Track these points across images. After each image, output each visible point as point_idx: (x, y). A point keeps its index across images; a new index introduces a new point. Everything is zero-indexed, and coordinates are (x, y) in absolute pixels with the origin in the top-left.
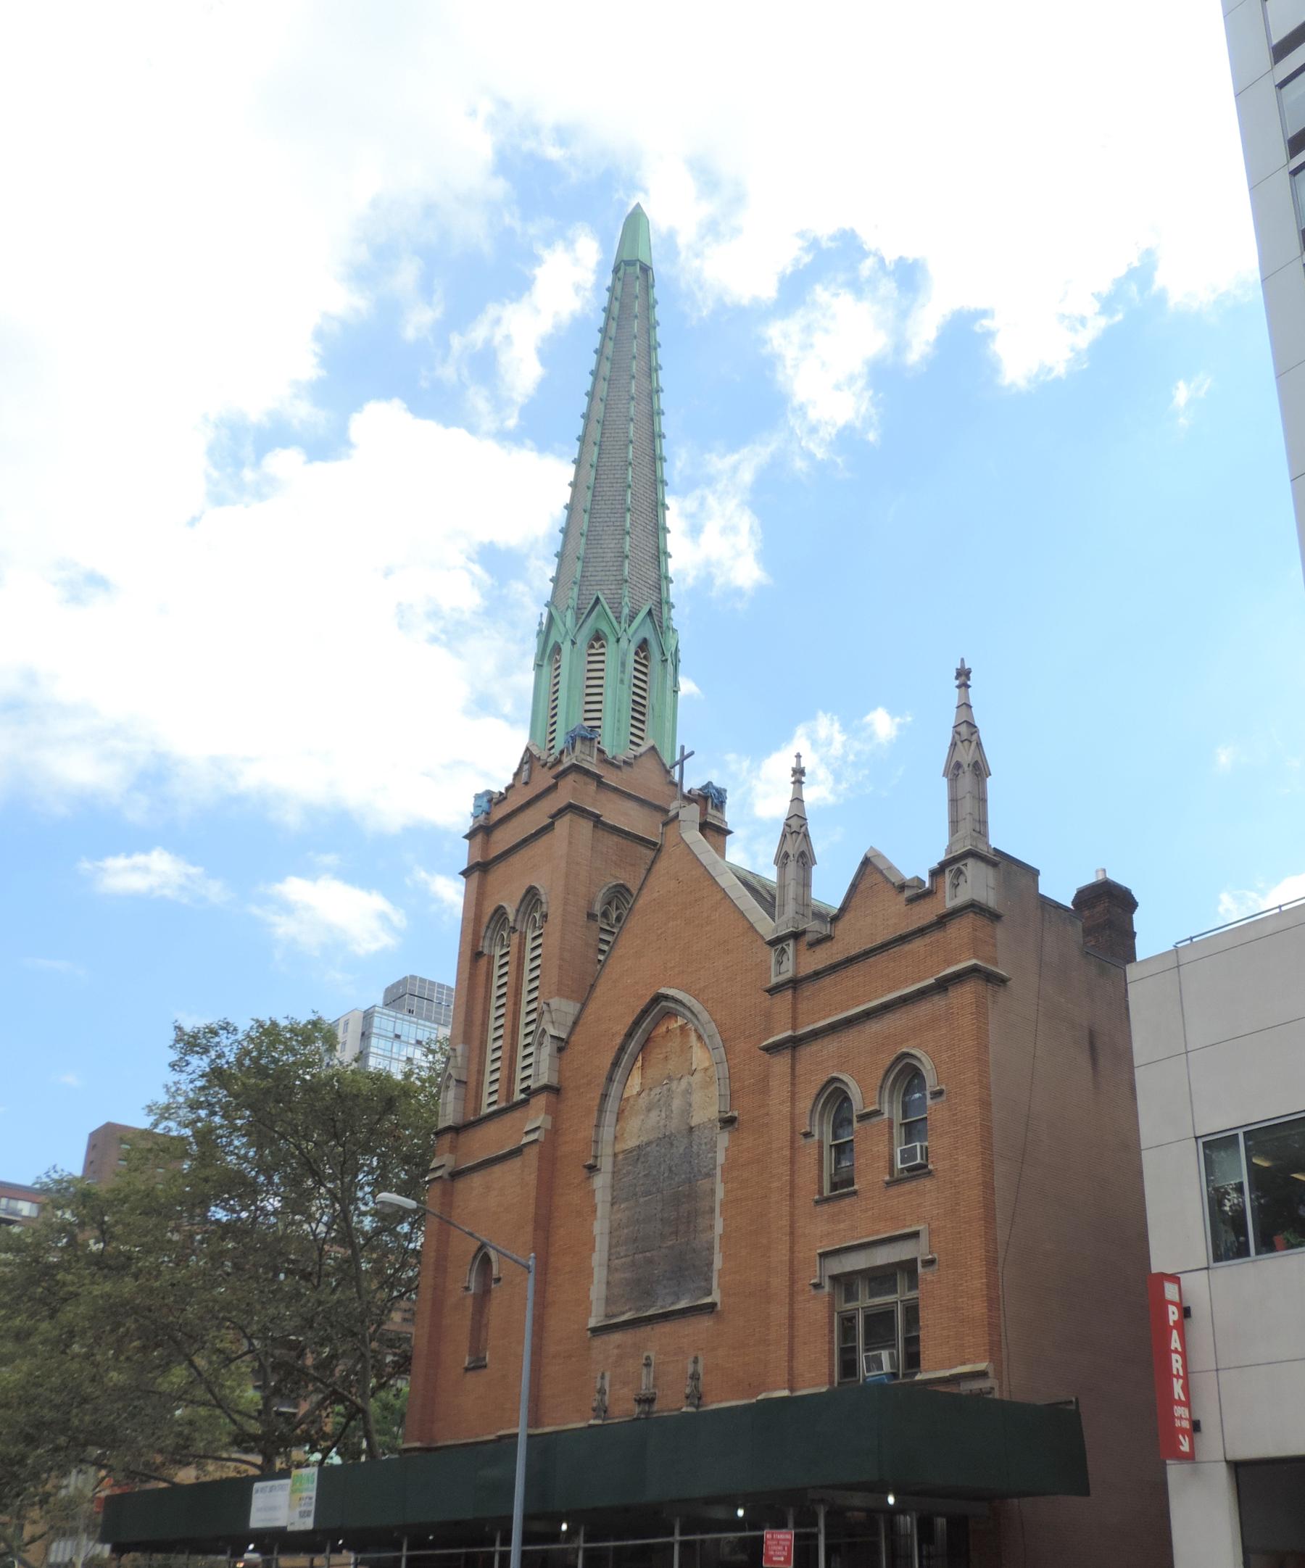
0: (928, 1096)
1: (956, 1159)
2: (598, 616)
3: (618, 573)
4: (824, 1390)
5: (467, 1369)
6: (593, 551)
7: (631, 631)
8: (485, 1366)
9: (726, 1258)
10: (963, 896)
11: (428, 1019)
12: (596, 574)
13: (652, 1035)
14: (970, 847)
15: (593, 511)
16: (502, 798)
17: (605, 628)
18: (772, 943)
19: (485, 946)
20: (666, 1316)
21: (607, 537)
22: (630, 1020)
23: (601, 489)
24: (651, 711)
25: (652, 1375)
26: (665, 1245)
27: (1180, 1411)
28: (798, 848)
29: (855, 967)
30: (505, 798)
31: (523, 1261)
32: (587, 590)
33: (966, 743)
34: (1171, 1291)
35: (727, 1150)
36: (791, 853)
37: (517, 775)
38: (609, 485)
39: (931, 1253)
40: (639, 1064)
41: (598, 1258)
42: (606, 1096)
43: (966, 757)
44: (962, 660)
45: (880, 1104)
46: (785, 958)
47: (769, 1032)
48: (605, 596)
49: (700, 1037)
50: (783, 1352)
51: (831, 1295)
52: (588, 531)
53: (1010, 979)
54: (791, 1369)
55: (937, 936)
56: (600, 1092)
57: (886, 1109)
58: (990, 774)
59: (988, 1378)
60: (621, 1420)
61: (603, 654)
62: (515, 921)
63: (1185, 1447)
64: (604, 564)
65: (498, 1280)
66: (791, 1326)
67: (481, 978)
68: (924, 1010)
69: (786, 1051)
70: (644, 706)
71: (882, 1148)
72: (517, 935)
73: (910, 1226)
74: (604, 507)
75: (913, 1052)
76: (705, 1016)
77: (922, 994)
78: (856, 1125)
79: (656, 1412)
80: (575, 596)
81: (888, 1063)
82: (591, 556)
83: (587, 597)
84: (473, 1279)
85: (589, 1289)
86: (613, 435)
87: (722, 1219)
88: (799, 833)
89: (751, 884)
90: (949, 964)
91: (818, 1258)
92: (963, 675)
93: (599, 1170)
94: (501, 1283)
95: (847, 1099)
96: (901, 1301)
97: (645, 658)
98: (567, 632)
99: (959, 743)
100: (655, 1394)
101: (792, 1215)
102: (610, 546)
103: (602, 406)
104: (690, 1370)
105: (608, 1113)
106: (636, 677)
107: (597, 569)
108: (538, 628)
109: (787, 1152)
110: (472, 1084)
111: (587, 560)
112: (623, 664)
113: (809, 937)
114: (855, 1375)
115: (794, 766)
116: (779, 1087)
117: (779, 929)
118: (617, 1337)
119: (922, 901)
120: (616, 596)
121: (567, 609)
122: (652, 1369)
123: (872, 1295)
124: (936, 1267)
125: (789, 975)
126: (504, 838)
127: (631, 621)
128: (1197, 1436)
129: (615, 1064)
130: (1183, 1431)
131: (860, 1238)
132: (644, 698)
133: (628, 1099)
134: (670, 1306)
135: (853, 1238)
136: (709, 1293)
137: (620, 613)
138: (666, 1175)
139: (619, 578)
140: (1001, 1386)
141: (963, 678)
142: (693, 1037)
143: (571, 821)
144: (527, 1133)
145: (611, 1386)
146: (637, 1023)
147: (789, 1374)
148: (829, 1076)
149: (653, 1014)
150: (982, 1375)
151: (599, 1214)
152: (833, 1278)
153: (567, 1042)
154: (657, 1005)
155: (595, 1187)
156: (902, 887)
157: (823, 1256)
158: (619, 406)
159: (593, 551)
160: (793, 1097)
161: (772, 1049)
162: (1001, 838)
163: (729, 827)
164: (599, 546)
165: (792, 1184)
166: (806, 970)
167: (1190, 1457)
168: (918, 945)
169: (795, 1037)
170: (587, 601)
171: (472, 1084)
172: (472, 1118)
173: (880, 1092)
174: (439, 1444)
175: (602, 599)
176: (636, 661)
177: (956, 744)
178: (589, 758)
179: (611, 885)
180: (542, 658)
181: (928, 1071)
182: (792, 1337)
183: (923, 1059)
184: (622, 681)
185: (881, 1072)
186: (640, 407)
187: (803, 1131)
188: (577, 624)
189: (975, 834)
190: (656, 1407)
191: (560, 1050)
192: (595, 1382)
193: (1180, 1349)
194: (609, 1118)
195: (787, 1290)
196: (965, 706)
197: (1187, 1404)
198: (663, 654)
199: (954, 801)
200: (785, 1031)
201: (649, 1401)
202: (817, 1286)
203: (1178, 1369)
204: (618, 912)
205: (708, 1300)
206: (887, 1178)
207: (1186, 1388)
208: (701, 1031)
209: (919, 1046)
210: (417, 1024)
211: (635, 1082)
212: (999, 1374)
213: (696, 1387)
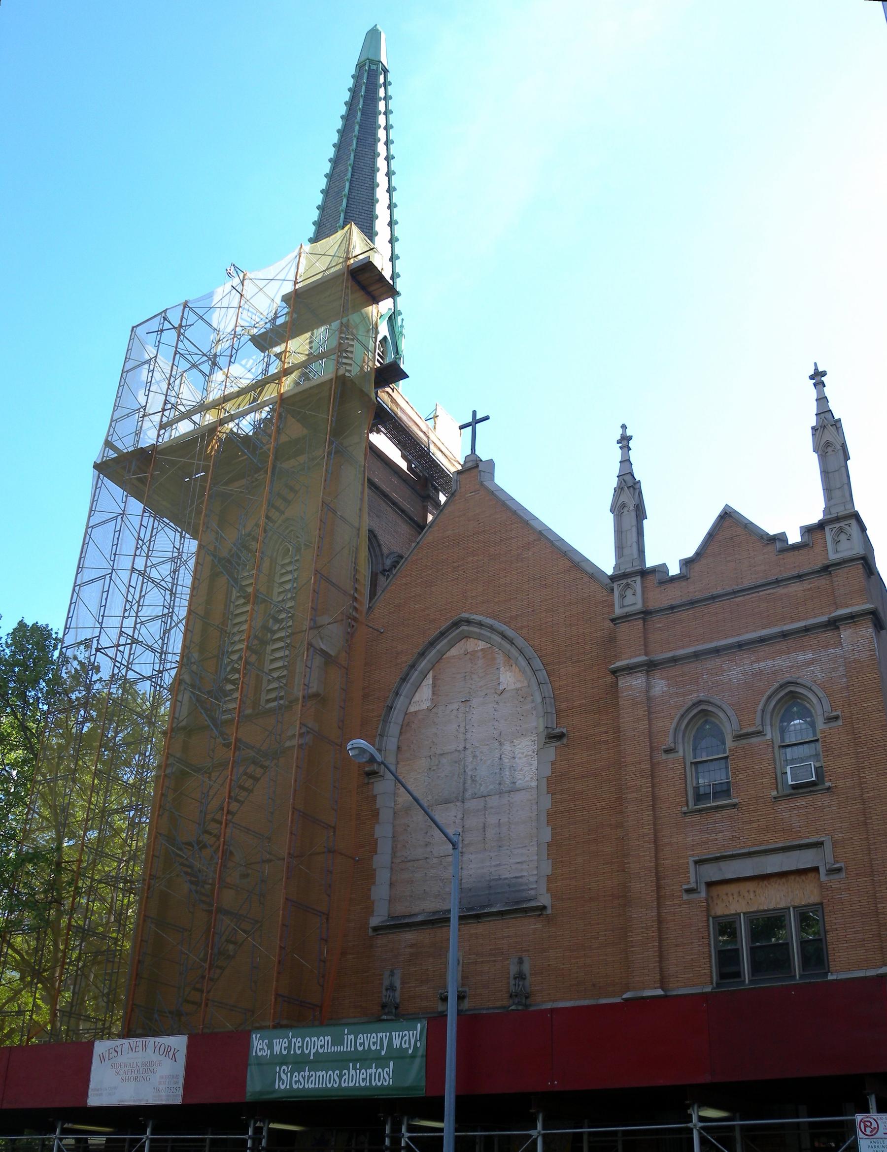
4: (708, 989)
40: (429, 680)
42: (391, 708)
44: (815, 364)
45: (763, 726)
57: (768, 730)
73: (807, 837)
86: (361, 178)
92: (625, 441)
96: (794, 908)
104: (513, 969)
125: (639, 606)
145: (403, 983)
149: (450, 637)
154: (457, 629)
158: (366, 159)
195: (654, 894)
206: (774, 793)
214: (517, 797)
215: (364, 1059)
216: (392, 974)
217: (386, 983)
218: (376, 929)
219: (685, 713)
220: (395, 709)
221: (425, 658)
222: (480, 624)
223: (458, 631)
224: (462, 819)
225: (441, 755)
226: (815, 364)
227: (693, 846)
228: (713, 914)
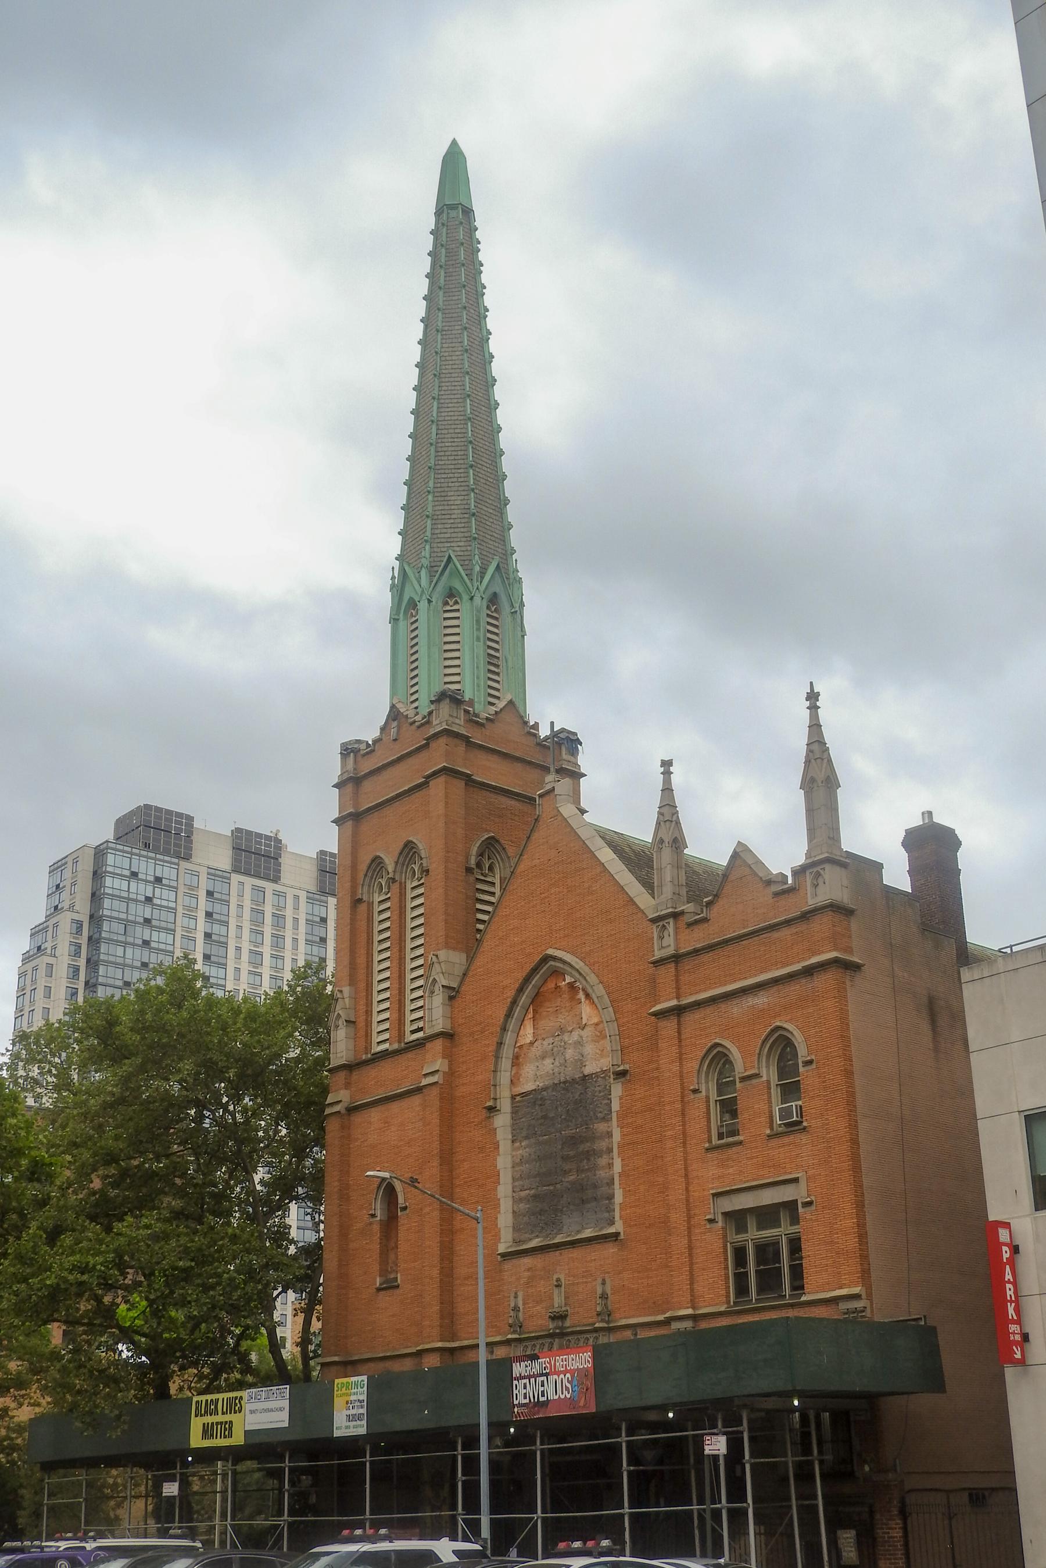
0: (801, 1064)
1: (827, 1119)
2: (451, 574)
3: (465, 530)
5: (379, 1290)
7: (482, 588)
8: (398, 1286)
9: (626, 1193)
11: (166, 852)
13: (541, 990)
16: (371, 749)
17: (458, 585)
18: (654, 921)
19: (362, 893)
20: (573, 1244)
21: (452, 493)
22: (521, 975)
24: (505, 664)
25: (563, 1295)
26: (567, 1180)
27: (1013, 1328)
29: (730, 948)
30: (373, 751)
31: (473, 1214)
34: (1003, 1235)
35: (621, 1098)
37: (383, 729)
38: (450, 440)
39: (809, 1196)
40: (530, 1015)
41: (504, 1190)
43: (820, 776)
44: (811, 683)
46: (666, 933)
48: (456, 554)
49: (588, 996)
51: (724, 1229)
53: (863, 965)
54: (692, 1290)
55: (802, 927)
56: (496, 1039)
57: (764, 1072)
60: (537, 1334)
61: (458, 610)
62: (394, 872)
63: (1018, 1356)
65: (405, 1208)
66: (690, 1255)
67: (362, 924)
68: (794, 989)
69: (672, 1017)
72: (397, 885)
73: (790, 1173)
74: (447, 462)
75: (785, 1026)
76: (592, 978)
77: (791, 977)
78: (738, 1085)
79: (569, 1327)
83: (439, 555)
84: (378, 1206)
85: (497, 1218)
87: (620, 1159)
88: (672, 821)
89: (618, 844)
91: (711, 1196)
94: (408, 1211)
97: (496, 610)
98: (423, 591)
99: (813, 761)
100: (567, 1311)
104: (599, 1291)
105: (503, 1059)
108: (391, 582)
109: (678, 1106)
110: (361, 1024)
111: (436, 517)
112: (478, 621)
116: (668, 1050)
118: (527, 1261)
123: (759, 1229)
125: (671, 951)
126: (375, 792)
127: (482, 578)
128: (1026, 1345)
129: (509, 1015)
130: (1016, 1343)
131: (748, 1181)
134: (577, 1234)
136: (612, 1222)
138: (563, 1117)
139: (466, 535)
140: (872, 1305)
142: (581, 996)
143: (446, 782)
144: (426, 1075)
145: (524, 1304)
146: (527, 979)
147: (692, 1296)
148: (713, 1041)
149: (542, 972)
150: (856, 1297)
151: (501, 1149)
152: (726, 1214)
153: (458, 992)
155: (496, 1126)
156: (769, 883)
157: (716, 1195)
162: (851, 842)
163: (583, 770)
164: (446, 503)
165: (684, 1133)
167: (1022, 1362)
168: (785, 933)
169: (680, 1005)
171: (361, 1024)
172: (364, 1057)
173: (759, 1058)
174: (356, 1358)
176: (488, 615)
177: (810, 761)
178: (457, 721)
180: (398, 613)
183: (795, 1033)
187: (692, 1088)
188: (431, 584)
191: (451, 998)
192: (509, 1301)
193: (1012, 1280)
194: (505, 1064)
197: (1018, 1322)
198: (512, 606)
200: (670, 1000)
201: (561, 1317)
202: (711, 1221)
203: (1010, 1295)
204: (491, 861)
205: (612, 1230)
206: (768, 1132)
207: (1017, 1310)
208: (590, 991)
209: (790, 1021)
210: (155, 859)
211: (528, 1033)
216: (516, 1297)
217: (512, 1305)
218: (504, 1255)
219: (705, 1055)
221: (524, 994)
226: (811, 683)
227: (713, 1179)
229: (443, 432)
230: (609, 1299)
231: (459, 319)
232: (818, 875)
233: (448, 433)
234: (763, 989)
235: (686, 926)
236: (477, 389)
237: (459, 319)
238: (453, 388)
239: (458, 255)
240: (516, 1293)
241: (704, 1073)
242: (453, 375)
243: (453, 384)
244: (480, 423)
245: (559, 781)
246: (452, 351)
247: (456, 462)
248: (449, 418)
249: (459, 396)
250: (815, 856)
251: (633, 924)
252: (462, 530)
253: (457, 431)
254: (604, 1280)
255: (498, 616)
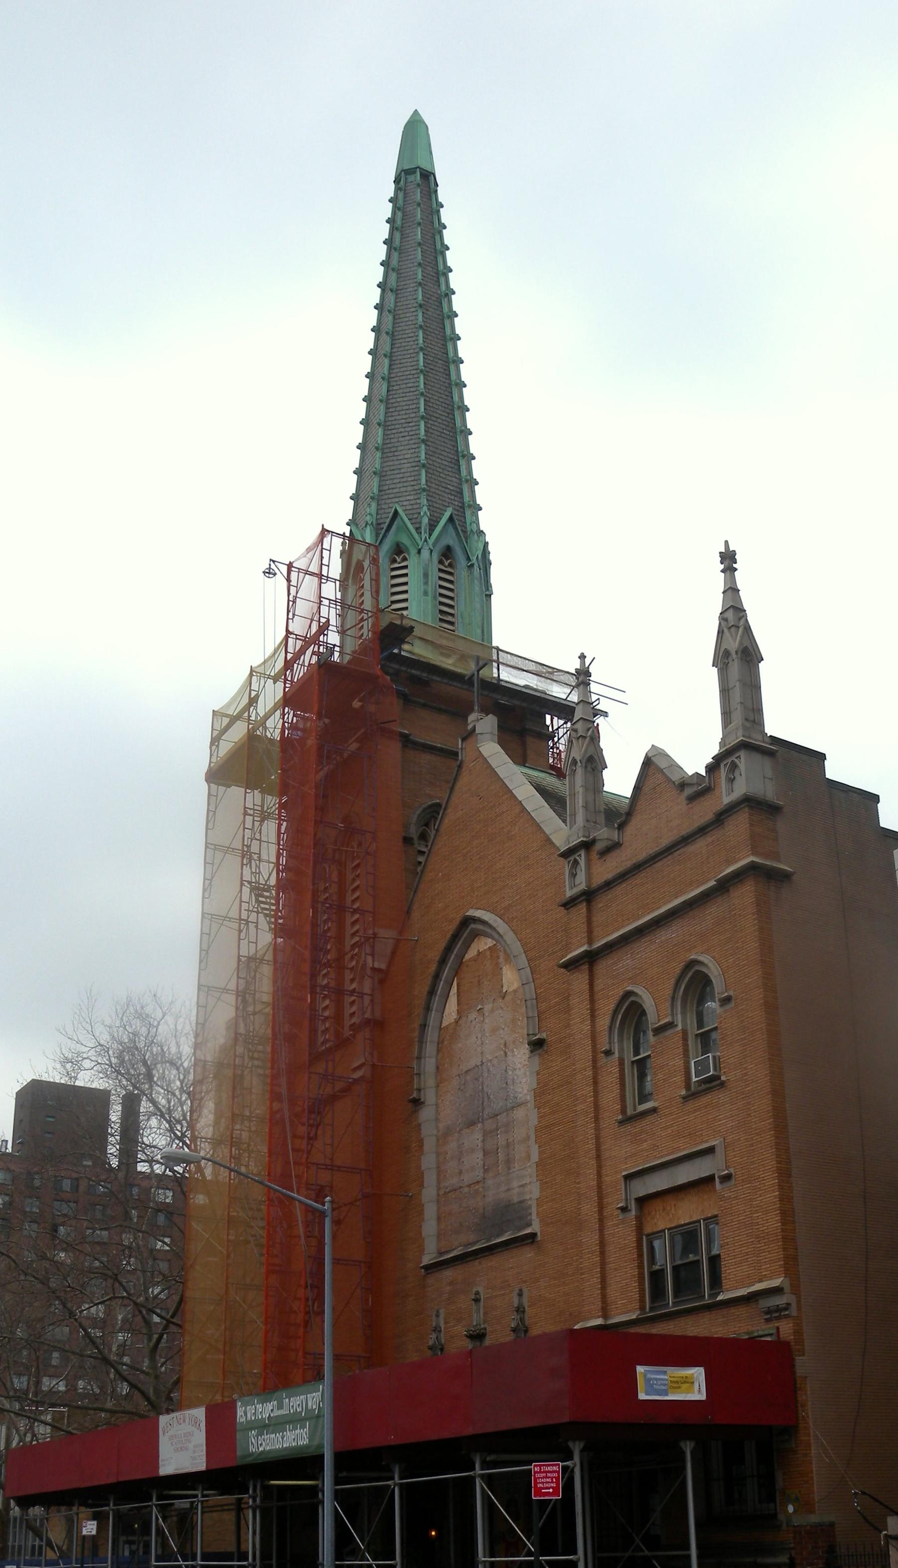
1: (746, 1068)
2: (398, 529)
3: (415, 483)
6: (388, 464)
7: (431, 541)
10: (740, 789)
12: (394, 486)
14: (742, 738)
15: (388, 424)
17: (405, 540)
18: (566, 854)
21: (402, 448)
23: (394, 400)
28: (586, 751)
32: (386, 504)
33: (733, 629)
36: (578, 759)
39: (727, 1168)
42: (425, 1025)
44: (726, 542)
47: (568, 948)
50: (596, 1280)
52: (384, 444)
54: (604, 1297)
58: (762, 660)
59: (784, 1293)
64: (401, 475)
66: (602, 1253)
70: (452, 615)
71: (679, 1062)
73: (707, 1141)
74: (398, 418)
75: (701, 958)
80: (374, 511)
81: (678, 971)
82: (388, 469)
88: (585, 737)
90: (729, 863)
91: (623, 1179)
92: (728, 559)
93: (423, 1103)
95: (644, 1013)
96: (704, 1220)
97: (450, 565)
99: (726, 630)
100: (485, 1329)
101: (598, 1138)
102: (406, 456)
103: (391, 318)
105: (428, 1043)
106: (441, 587)
107: (395, 481)
108: (341, 548)
109: (590, 1073)
113: (599, 846)
114: (665, 1300)
115: (578, 667)
117: (727, 743)
118: (448, 1274)
119: (702, 799)
120: (415, 507)
121: (366, 526)
122: (482, 1304)
124: (733, 1182)
125: (583, 887)
131: (662, 1157)
132: (452, 607)
133: (447, 1027)
135: (655, 1158)
137: (420, 523)
139: (416, 488)
140: (799, 1302)
141: (727, 563)
145: (446, 1323)
150: (777, 1291)
151: (426, 1147)
156: (683, 784)
157: (629, 1178)
159: (388, 464)
160: (593, 1016)
161: (571, 965)
164: (395, 458)
166: (598, 881)
168: (700, 846)
170: (387, 515)
175: (400, 510)
176: (440, 570)
179: (424, 806)
181: (715, 976)
182: (603, 1264)
183: (710, 965)
184: (426, 593)
185: (673, 981)
186: (430, 313)
189: (747, 724)
190: (487, 1342)
191: (382, 982)
196: (732, 591)
198: (469, 559)
199: (725, 691)
202: (624, 1209)
206: (683, 1092)
212: (796, 1290)
213: (522, 1320)
214: (519, 1114)
215: (294, 1420)
216: (437, 1316)
217: (434, 1324)
220: (429, 1026)
222: (484, 923)
223: (468, 931)
224: (483, 1141)
225: (466, 1072)
228: (646, 1233)
229: (395, 388)
230: (526, 1314)
231: (415, 276)
232: (734, 767)
233: (400, 389)
234: (678, 917)
235: (599, 856)
236: (433, 343)
237: (415, 276)
238: (406, 344)
239: (415, 216)
240: (438, 1311)
241: (616, 1030)
242: (407, 332)
243: (407, 340)
244: (436, 377)
245: (482, 719)
246: (406, 309)
247: (407, 416)
248: (401, 374)
249: (412, 351)
250: (730, 744)
251: (551, 866)
252: (412, 483)
253: (409, 385)
254: (521, 1290)
255: (453, 571)
